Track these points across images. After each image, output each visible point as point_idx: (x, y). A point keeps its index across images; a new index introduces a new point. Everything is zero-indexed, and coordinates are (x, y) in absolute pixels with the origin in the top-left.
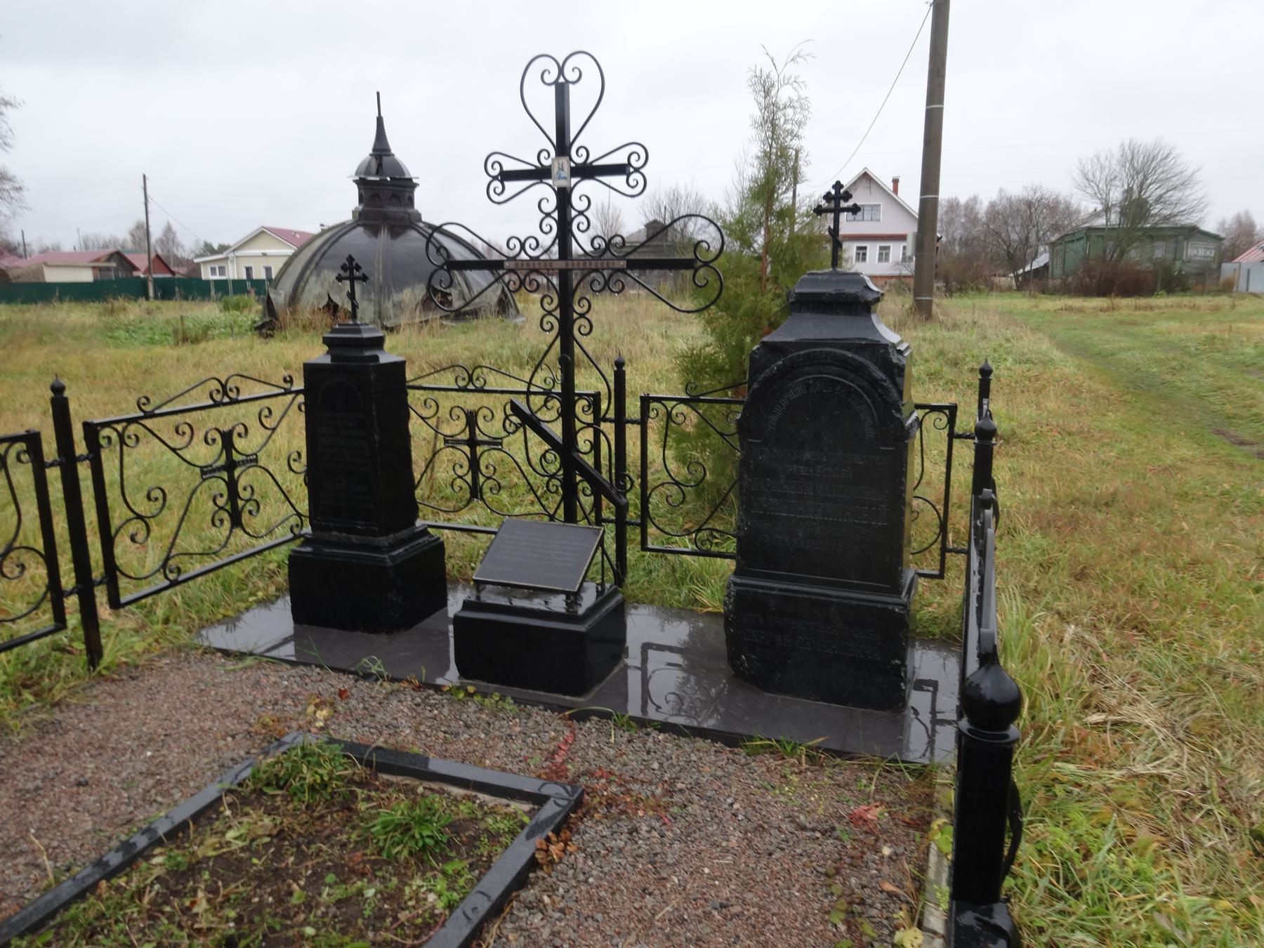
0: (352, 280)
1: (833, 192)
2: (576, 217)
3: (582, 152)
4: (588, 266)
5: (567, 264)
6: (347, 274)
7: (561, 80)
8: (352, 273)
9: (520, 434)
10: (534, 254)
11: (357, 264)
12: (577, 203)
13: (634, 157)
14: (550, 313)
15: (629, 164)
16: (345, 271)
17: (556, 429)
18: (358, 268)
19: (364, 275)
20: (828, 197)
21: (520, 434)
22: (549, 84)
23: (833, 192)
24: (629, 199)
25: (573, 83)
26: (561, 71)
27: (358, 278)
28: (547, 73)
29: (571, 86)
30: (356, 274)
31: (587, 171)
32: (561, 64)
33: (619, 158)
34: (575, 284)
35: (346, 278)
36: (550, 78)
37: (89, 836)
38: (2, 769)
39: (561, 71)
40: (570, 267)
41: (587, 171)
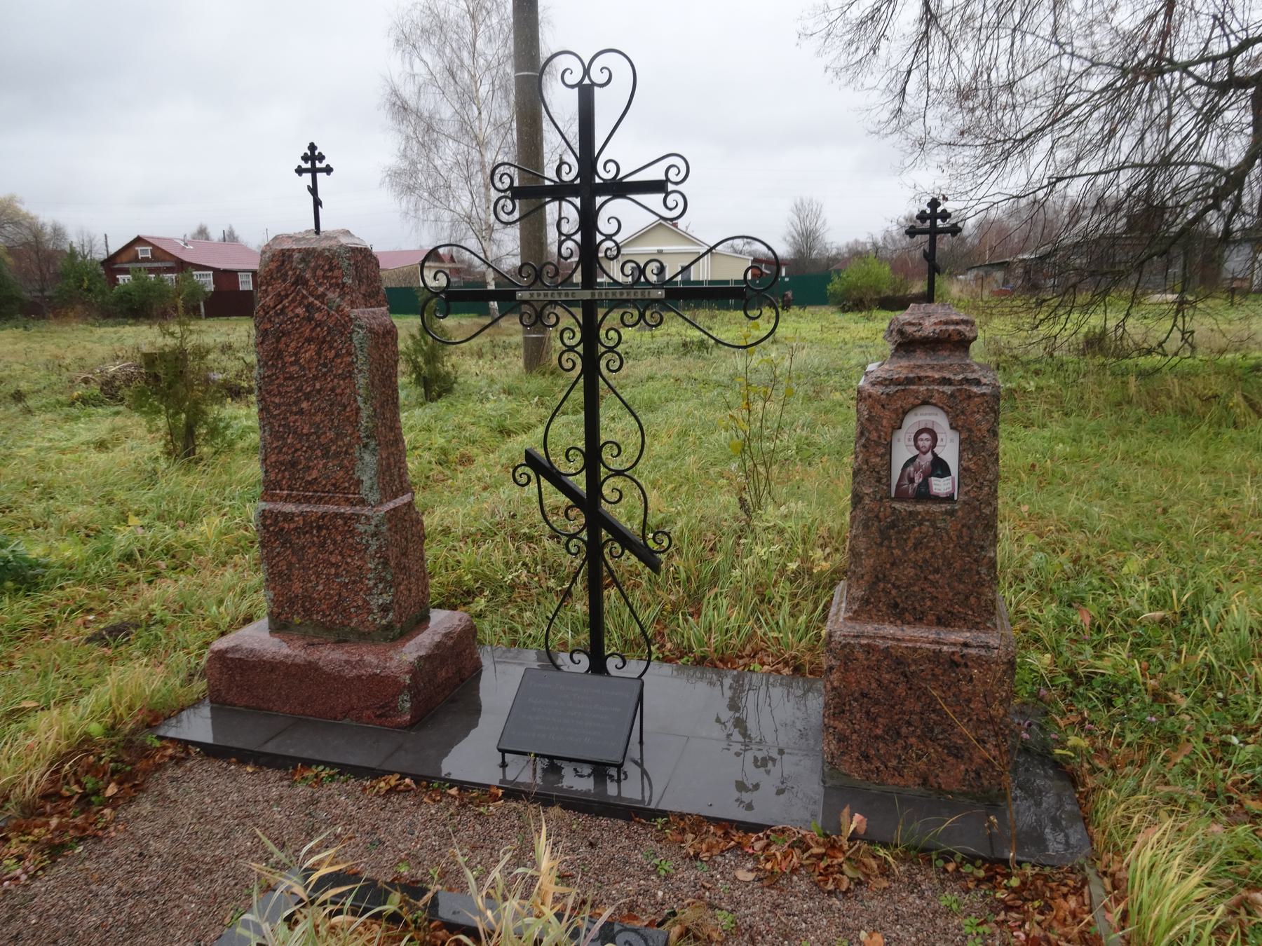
0: (314, 171)
1: (928, 211)
2: (602, 242)
3: (611, 166)
4: (618, 296)
5: (593, 294)
6: (309, 165)
7: (587, 81)
8: (313, 164)
9: (533, 486)
10: (603, 363)
11: (320, 153)
12: (605, 225)
13: (673, 172)
14: (571, 349)
15: (668, 180)
16: (306, 162)
17: (580, 483)
18: (321, 158)
19: (328, 166)
20: (922, 216)
21: (533, 486)
22: (572, 87)
23: (928, 211)
24: (554, 51)
25: (602, 86)
26: (587, 72)
27: (321, 170)
28: (569, 72)
29: (596, 88)
30: (318, 165)
31: (620, 188)
32: (586, 65)
33: (655, 174)
34: (600, 317)
35: (306, 171)
36: (573, 78)
37: (56, 388)
38: (3, 619)
39: (587, 72)
40: (597, 297)
41: (620, 188)
